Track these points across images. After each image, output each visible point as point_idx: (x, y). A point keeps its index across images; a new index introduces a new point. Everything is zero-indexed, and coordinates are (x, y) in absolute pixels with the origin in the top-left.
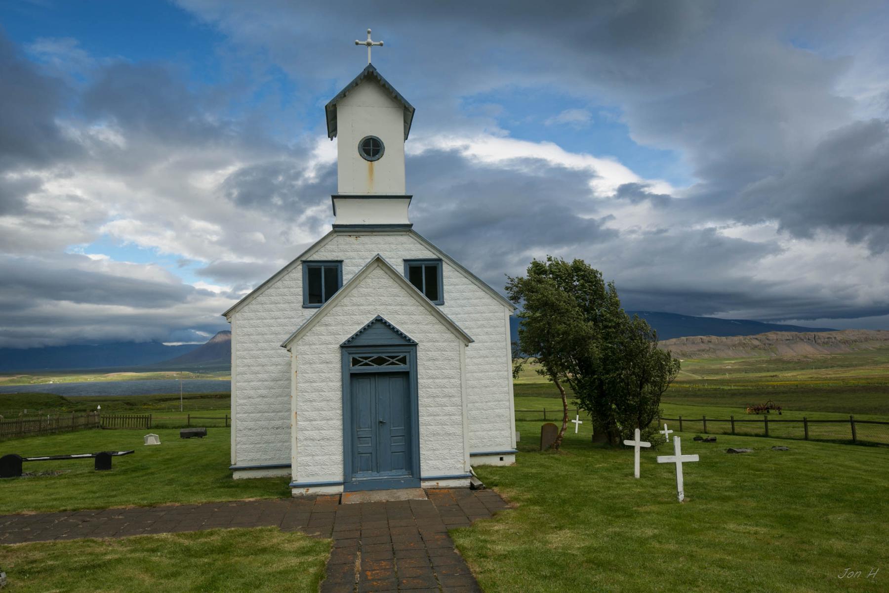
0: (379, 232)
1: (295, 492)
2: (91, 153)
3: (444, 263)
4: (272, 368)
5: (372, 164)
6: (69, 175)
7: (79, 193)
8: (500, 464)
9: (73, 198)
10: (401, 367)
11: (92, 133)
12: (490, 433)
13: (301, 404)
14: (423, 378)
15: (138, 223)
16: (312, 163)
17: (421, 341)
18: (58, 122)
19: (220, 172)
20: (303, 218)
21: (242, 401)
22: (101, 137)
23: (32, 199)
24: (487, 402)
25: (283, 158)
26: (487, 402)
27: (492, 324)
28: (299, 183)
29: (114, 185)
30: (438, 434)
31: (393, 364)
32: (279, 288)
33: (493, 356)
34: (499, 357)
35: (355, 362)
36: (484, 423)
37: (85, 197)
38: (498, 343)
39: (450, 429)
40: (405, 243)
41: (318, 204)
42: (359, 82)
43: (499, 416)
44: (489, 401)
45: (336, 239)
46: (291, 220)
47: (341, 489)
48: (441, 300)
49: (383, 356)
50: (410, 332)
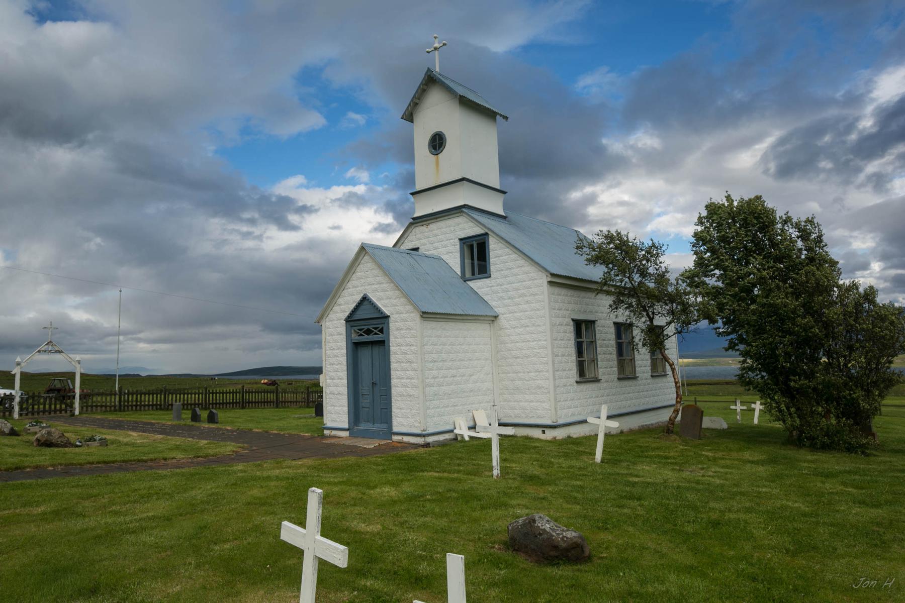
0: (441, 217)
1: (326, 432)
2: (634, 160)
3: (490, 236)
5: (437, 158)
6: (618, 184)
7: (626, 198)
8: (542, 437)
9: (622, 203)
10: (380, 337)
11: (631, 142)
12: (532, 404)
14: (393, 346)
15: (679, 216)
16: (869, 109)
17: (392, 314)
18: (605, 141)
19: (757, 147)
20: (862, 177)
22: (640, 145)
23: (592, 211)
24: (528, 372)
25: (832, 112)
26: (528, 372)
27: (532, 292)
28: (853, 137)
29: (655, 184)
30: (403, 395)
31: (376, 334)
33: (533, 325)
34: (538, 326)
36: (526, 394)
37: (633, 200)
38: (538, 312)
39: (411, 391)
40: (460, 224)
41: (882, 156)
42: (425, 87)
43: (540, 388)
44: (531, 372)
45: (414, 230)
46: (847, 182)
47: (346, 434)
48: (488, 273)
49: (370, 327)
50: (385, 306)
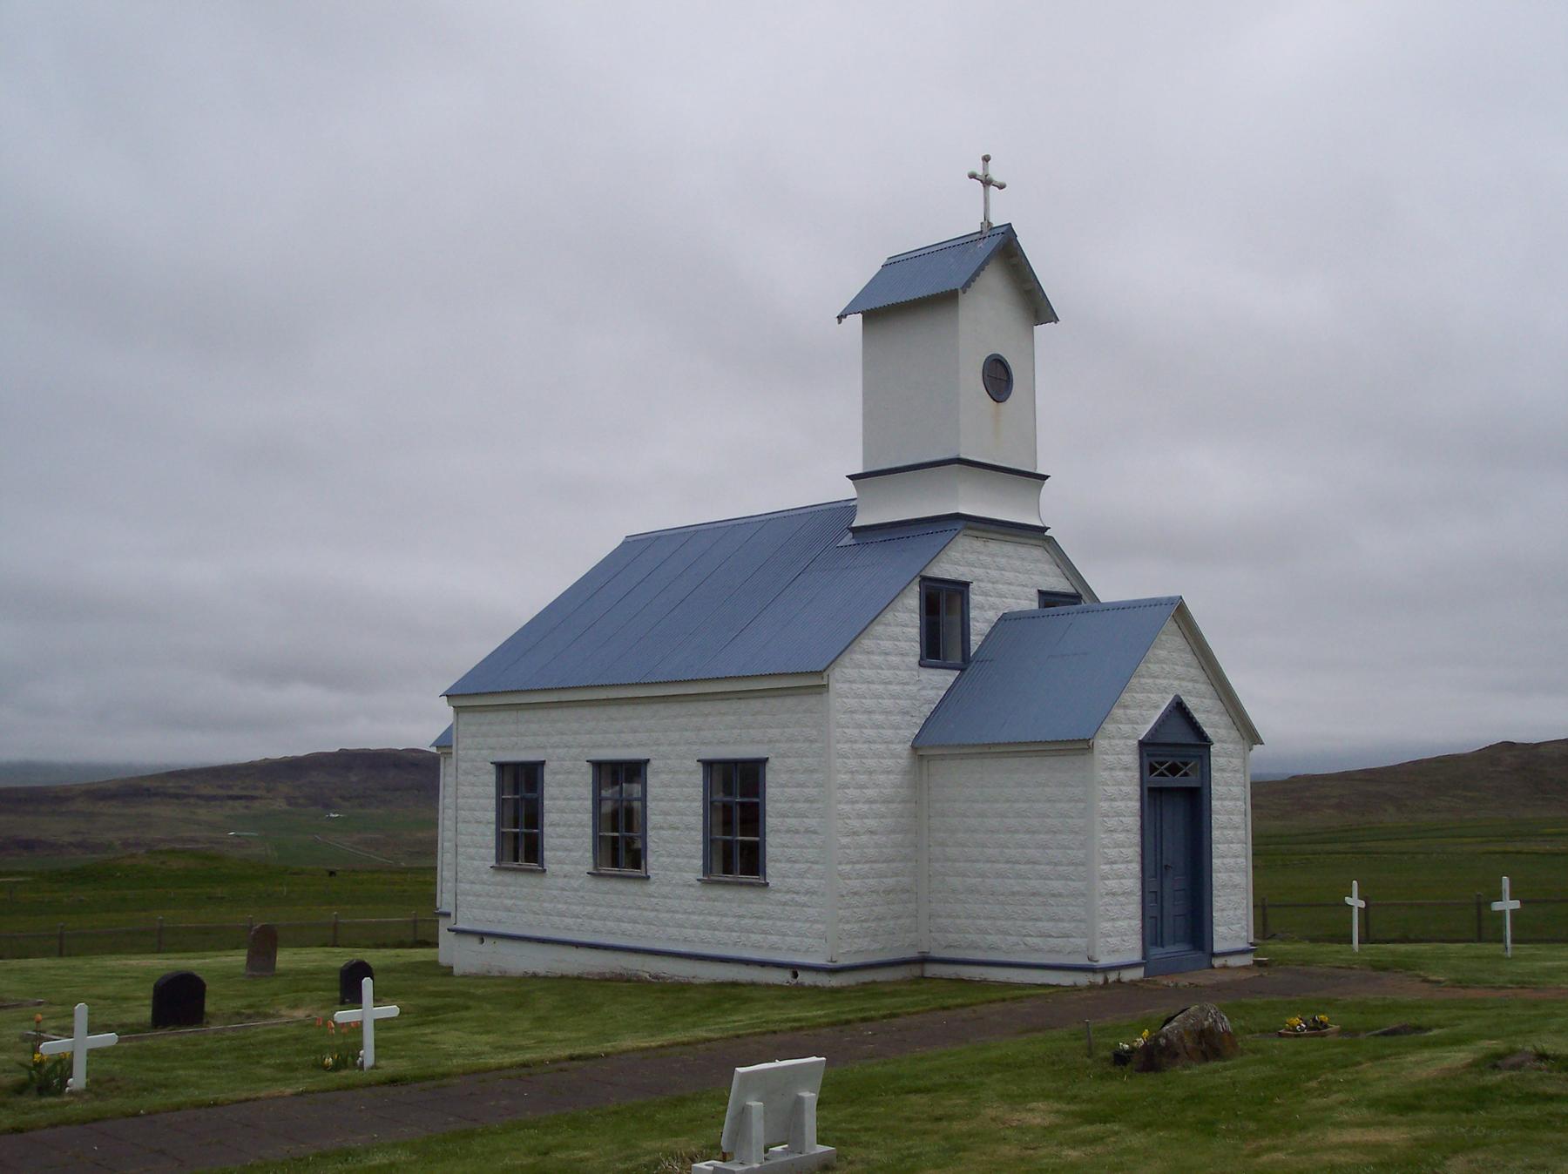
4: (882, 777)
13: (1103, 836)
21: (845, 841)
32: (889, 625)
35: (1152, 769)
